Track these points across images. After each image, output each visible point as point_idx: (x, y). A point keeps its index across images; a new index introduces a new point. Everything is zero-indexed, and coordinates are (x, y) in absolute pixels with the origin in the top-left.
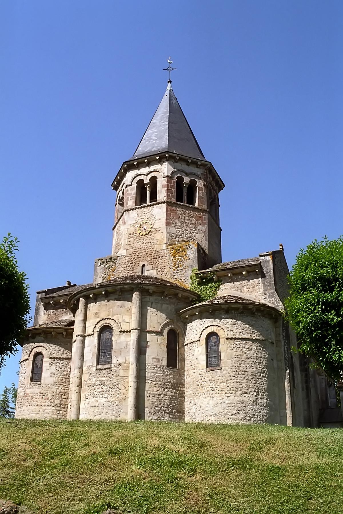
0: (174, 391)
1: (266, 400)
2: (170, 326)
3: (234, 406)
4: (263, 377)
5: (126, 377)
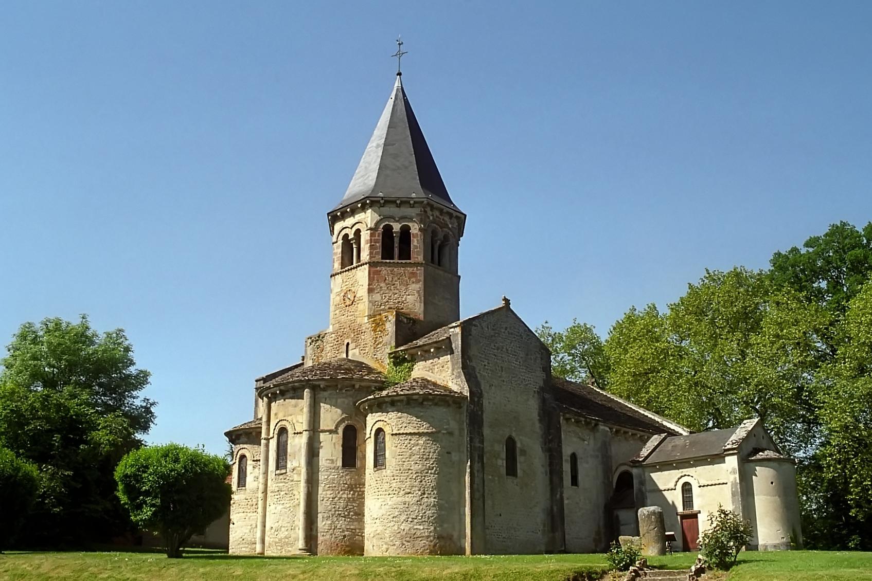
0: (351, 493)
1: (433, 499)
2: (346, 422)
4: (431, 473)
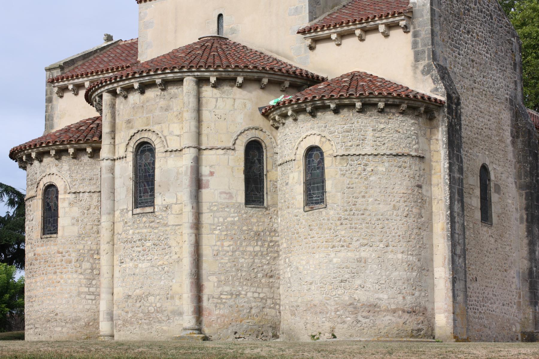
3: (347, 266)
5: (179, 227)
